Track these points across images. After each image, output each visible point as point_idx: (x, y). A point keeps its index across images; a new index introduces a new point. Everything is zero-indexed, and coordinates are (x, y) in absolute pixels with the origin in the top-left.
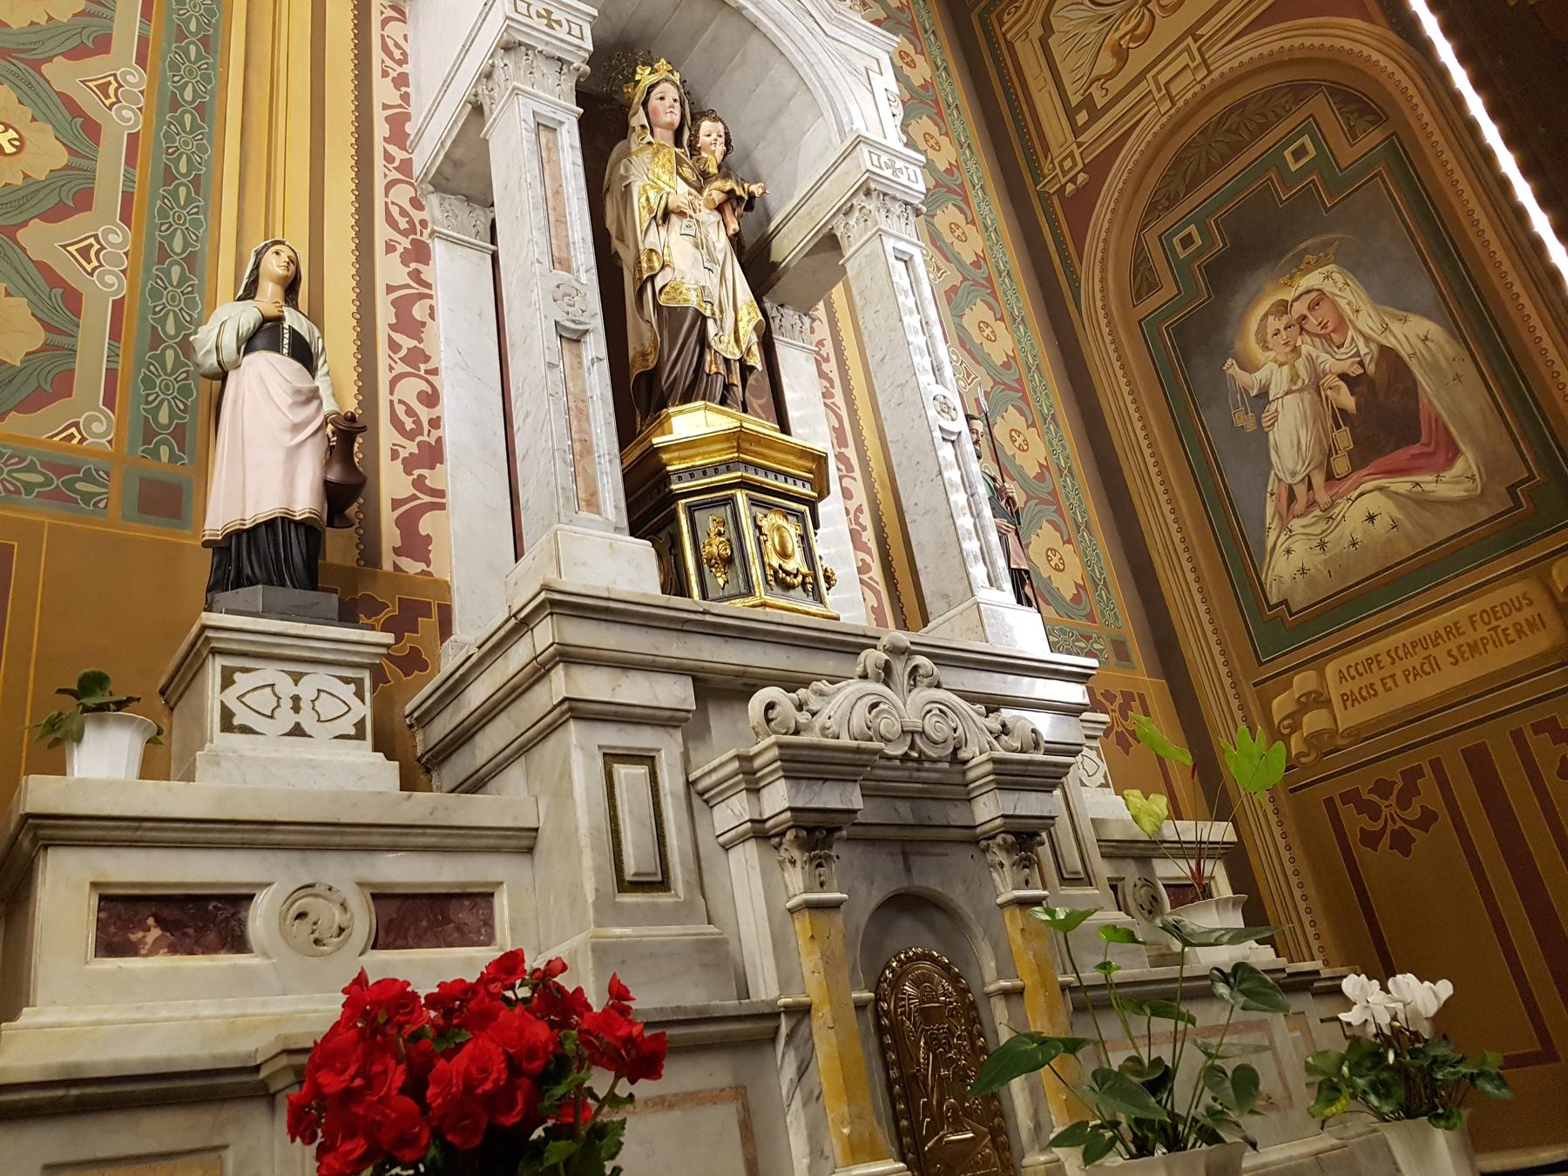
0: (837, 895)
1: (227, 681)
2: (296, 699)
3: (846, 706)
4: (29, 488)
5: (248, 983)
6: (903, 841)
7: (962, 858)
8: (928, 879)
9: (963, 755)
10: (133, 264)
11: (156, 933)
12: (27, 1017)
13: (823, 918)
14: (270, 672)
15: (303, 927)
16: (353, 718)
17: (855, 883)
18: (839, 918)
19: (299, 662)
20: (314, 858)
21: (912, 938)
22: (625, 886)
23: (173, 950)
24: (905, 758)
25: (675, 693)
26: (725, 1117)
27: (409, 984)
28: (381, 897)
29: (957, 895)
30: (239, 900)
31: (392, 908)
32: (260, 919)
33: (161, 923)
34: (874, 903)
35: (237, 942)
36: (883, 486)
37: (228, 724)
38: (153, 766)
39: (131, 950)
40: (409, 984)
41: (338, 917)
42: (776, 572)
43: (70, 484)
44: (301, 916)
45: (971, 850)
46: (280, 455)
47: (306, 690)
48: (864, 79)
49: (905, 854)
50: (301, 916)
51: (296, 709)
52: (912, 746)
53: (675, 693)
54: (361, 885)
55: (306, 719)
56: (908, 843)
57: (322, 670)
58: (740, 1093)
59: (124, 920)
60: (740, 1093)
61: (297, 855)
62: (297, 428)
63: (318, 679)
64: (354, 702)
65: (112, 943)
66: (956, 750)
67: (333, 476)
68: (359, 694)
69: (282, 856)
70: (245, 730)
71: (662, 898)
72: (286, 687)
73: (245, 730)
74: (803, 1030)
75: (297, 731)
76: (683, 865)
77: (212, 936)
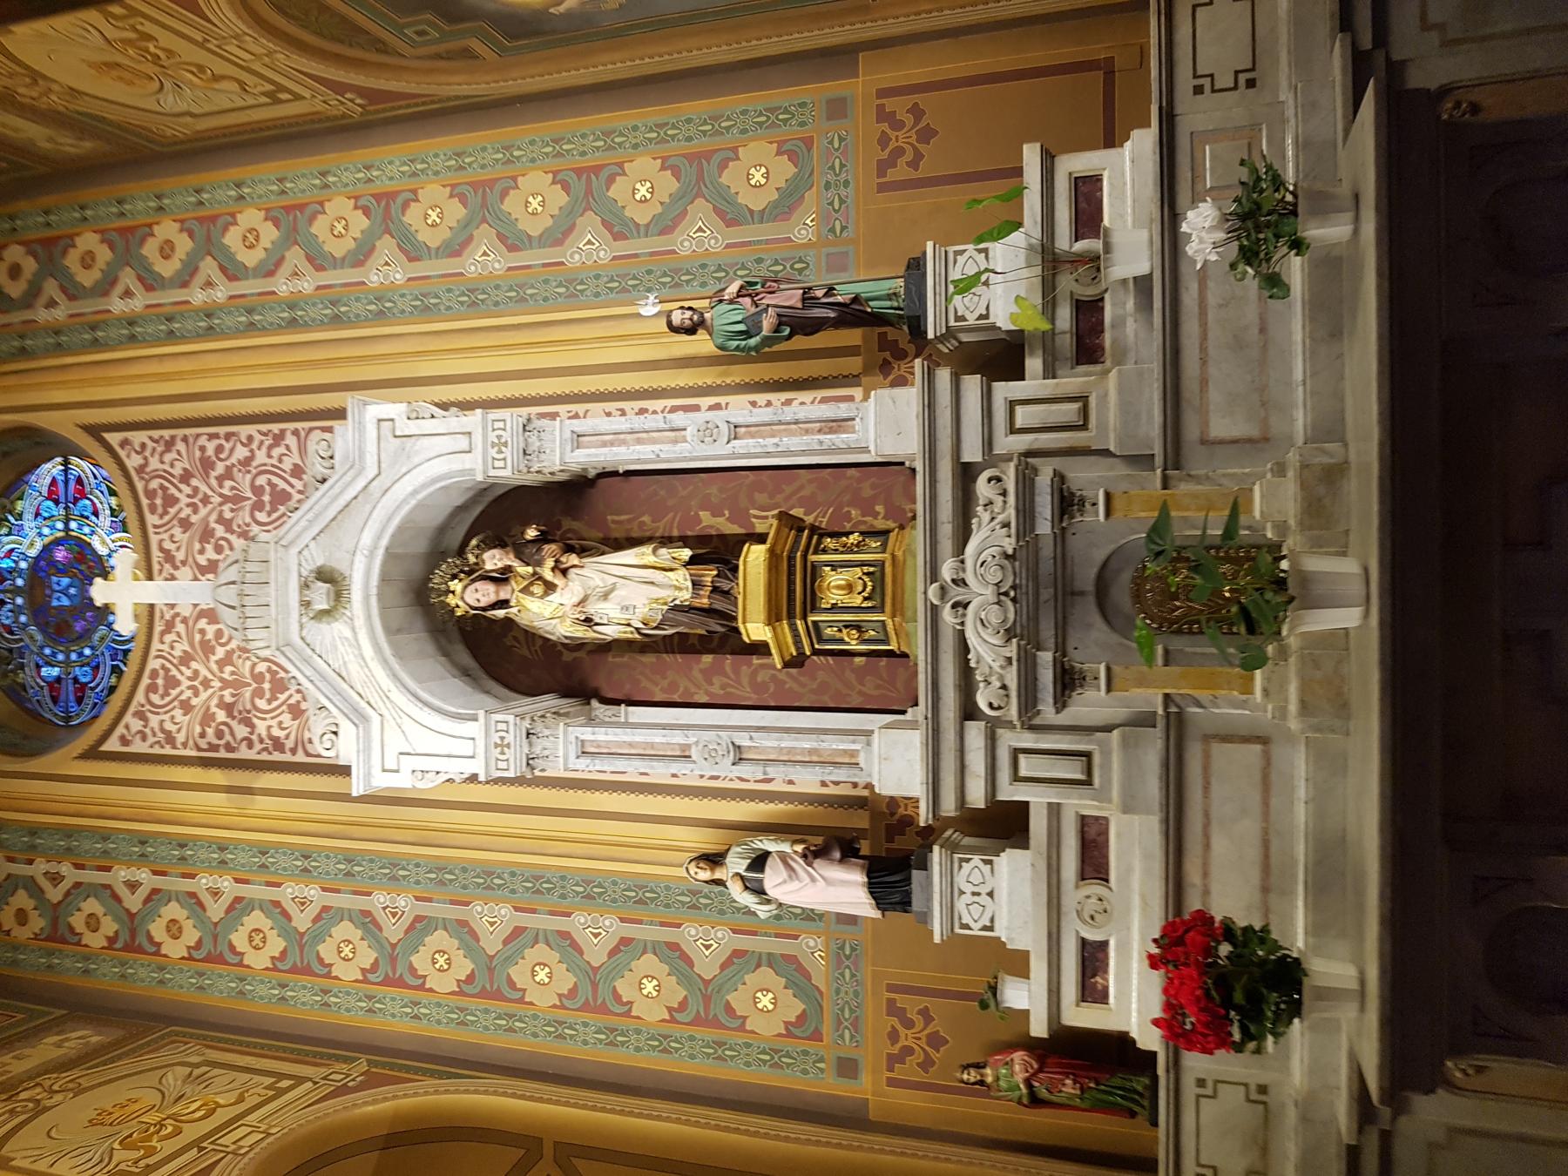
0: (1102, 668)
1: (967, 927)
2: (974, 894)
3: (985, 646)
4: (853, 976)
5: (1124, 947)
6: (1064, 595)
7: (1075, 543)
8: (1086, 578)
9: (1010, 552)
10: (707, 923)
11: (1098, 979)
12: (1134, 1034)
13: (1116, 682)
14: (960, 905)
15: (1097, 916)
16: (981, 865)
17: (1093, 645)
18: (1116, 669)
19: (952, 892)
20: (1064, 909)
21: (1121, 593)
22: (1088, 782)
23: (1106, 971)
24: (1014, 600)
25: (975, 733)
26: (1217, 748)
27: (1151, 957)
28: (1083, 876)
29: (1100, 555)
30: (1084, 943)
31: (1088, 869)
32: (1093, 935)
33: (1094, 976)
34: (1105, 628)
35: (1104, 945)
36: (726, 374)
37: (991, 929)
38: (1018, 964)
39: (1106, 989)
40: (1151, 957)
41: (1094, 900)
42: (866, 599)
43: (848, 958)
44: (1092, 918)
45: (1068, 535)
46: (831, 889)
47: (968, 889)
48: (409, 442)
49: (1073, 594)
50: (1092, 918)
51: (979, 894)
52: (1006, 594)
53: (975, 733)
54: (1077, 887)
55: (984, 890)
56: (1066, 593)
57: (956, 879)
58: (1207, 738)
59: (1092, 992)
60: (1207, 738)
61: (1063, 918)
62: (813, 880)
63: (961, 880)
64: (972, 864)
65: (1101, 997)
66: (1007, 556)
67: (837, 855)
68: (968, 861)
69: (1063, 924)
70: (992, 920)
71: (1097, 759)
72: (967, 898)
73: (992, 920)
74: (1178, 699)
75: (991, 894)
76: (1078, 743)
77: (1100, 955)
